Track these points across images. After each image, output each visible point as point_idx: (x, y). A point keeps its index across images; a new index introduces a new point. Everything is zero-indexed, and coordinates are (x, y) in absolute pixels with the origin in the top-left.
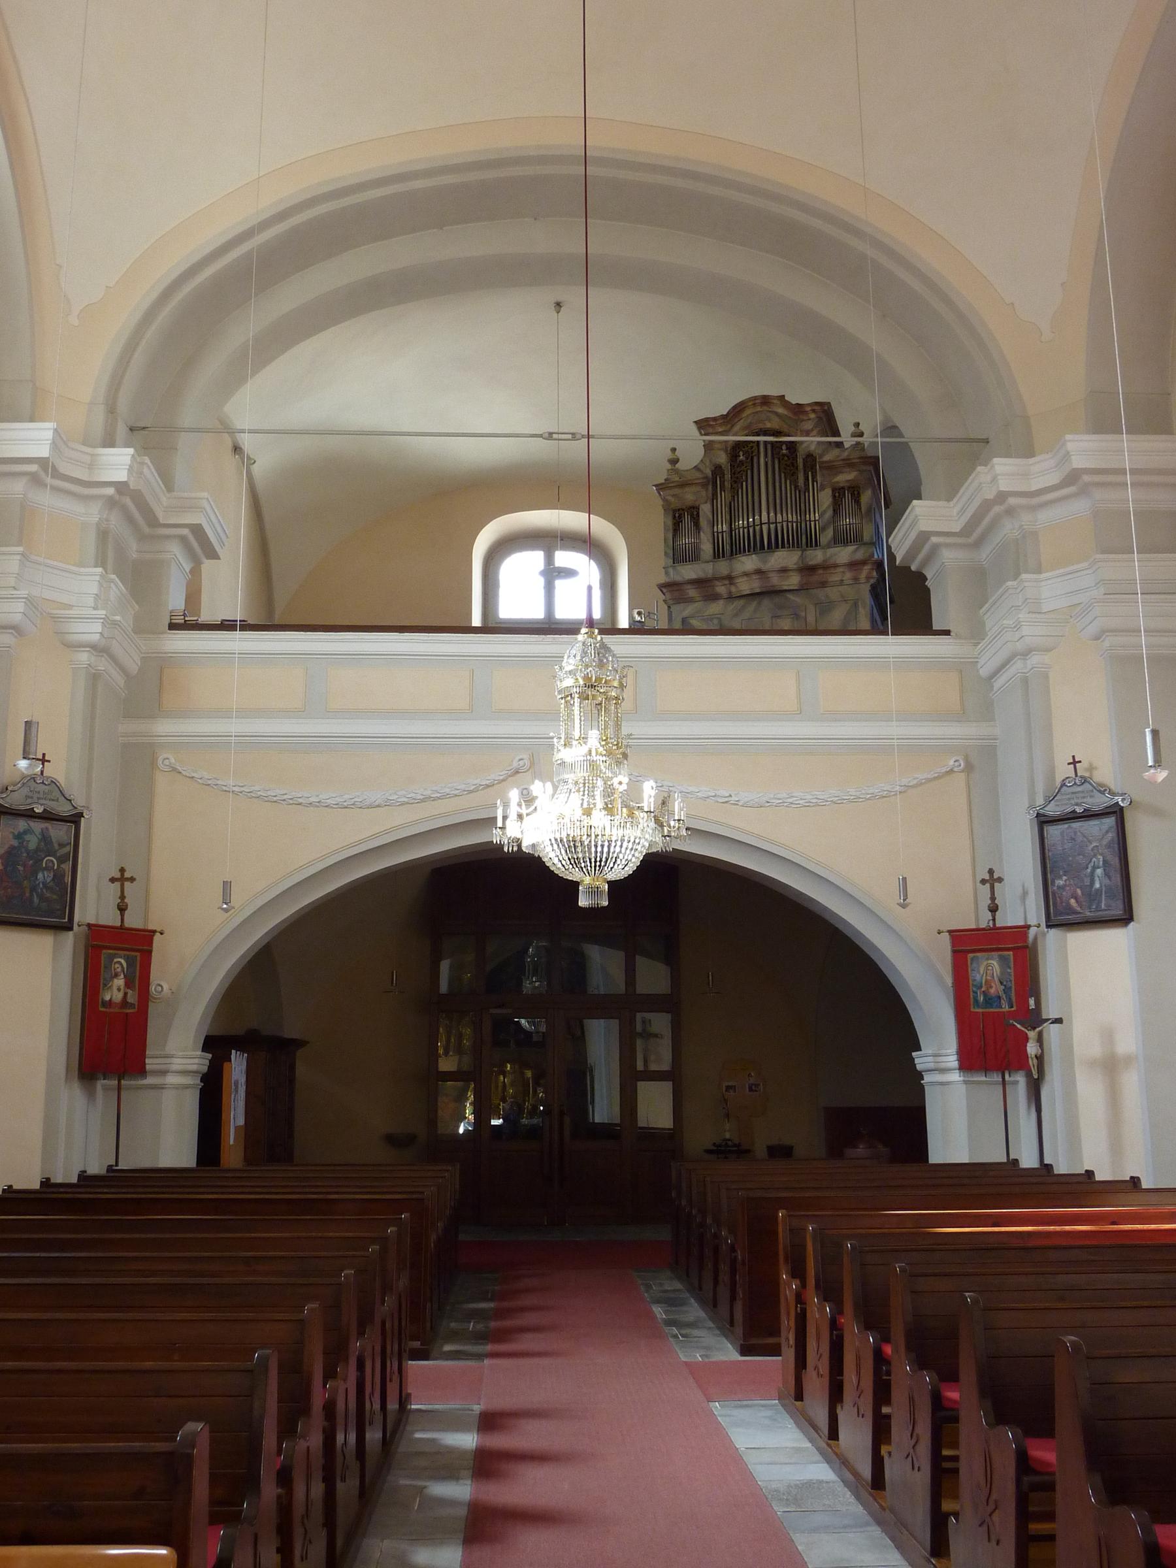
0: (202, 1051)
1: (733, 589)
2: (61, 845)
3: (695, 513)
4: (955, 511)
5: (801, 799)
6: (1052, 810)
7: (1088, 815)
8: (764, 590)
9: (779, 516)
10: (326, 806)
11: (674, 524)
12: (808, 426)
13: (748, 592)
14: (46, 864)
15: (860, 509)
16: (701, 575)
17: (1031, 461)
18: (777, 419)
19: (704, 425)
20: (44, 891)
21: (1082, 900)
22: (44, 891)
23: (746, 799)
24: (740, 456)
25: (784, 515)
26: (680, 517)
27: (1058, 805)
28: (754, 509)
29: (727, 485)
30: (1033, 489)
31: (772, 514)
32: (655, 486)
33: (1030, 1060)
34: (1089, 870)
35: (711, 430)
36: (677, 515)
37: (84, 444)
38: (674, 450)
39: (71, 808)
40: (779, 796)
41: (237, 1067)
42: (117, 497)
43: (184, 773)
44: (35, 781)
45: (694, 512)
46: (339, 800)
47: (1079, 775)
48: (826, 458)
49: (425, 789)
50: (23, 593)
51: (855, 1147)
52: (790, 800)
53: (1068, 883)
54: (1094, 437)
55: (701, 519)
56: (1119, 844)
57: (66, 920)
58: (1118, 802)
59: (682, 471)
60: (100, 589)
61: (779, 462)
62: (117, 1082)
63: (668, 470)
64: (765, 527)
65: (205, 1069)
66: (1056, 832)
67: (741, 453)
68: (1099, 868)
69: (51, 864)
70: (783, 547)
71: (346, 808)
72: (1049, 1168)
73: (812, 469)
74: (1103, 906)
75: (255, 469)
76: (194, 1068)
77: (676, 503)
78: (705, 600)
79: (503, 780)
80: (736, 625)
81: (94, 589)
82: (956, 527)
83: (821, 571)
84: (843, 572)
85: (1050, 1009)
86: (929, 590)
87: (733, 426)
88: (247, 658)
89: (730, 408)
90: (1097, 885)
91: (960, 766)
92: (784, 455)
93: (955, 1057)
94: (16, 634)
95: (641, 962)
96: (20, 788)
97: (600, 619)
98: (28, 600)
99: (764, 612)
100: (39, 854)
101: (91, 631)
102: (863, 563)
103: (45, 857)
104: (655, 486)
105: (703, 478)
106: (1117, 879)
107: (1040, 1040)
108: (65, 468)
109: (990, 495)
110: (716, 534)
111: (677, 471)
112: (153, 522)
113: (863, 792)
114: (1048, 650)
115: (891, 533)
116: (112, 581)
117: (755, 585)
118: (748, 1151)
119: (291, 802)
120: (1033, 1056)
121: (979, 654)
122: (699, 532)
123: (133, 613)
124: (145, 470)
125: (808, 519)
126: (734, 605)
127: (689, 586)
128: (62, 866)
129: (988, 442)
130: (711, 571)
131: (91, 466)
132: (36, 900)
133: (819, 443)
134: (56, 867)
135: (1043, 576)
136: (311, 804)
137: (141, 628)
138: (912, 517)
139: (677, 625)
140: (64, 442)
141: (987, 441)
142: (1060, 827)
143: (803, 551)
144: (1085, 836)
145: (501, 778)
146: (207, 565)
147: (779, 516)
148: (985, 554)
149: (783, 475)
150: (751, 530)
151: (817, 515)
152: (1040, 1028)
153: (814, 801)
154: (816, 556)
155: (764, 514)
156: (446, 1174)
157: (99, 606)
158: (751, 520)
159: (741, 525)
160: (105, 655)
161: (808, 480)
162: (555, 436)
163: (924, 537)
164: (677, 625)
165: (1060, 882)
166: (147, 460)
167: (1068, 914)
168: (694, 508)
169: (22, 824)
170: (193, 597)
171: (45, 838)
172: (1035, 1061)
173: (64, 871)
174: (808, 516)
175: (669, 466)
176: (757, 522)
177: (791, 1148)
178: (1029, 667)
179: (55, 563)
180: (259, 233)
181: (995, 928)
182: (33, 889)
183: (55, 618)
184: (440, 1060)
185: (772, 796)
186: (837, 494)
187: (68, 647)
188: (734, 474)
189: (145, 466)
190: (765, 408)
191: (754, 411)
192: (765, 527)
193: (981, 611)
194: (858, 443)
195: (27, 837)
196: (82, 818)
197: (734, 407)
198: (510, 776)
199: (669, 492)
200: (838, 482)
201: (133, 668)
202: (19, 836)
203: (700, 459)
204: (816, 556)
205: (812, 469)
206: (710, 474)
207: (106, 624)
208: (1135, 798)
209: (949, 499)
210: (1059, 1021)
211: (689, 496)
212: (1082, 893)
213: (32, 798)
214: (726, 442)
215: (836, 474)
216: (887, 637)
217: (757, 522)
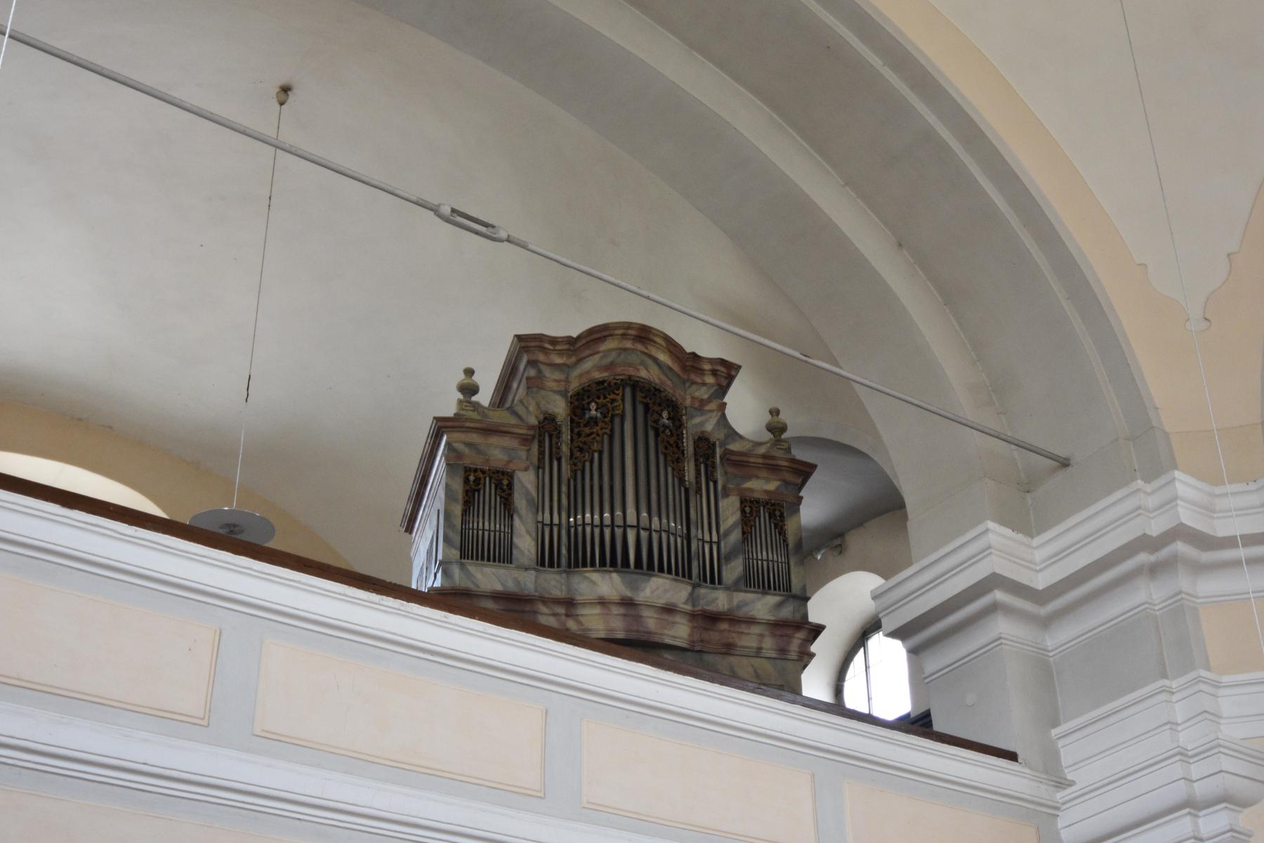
3: (505, 482)
8: (634, 636)
9: (655, 520)
11: (466, 492)
13: (602, 635)
16: (511, 587)
26: (477, 481)
35: (541, 357)
36: (472, 478)
45: (503, 482)
67: (593, 406)
73: (707, 459)
77: (472, 459)
83: (724, 626)
84: (761, 635)
87: (580, 361)
122: (511, 517)
154: (717, 599)
155: (631, 511)
158: (606, 515)
168: (503, 473)
186: (748, 509)
190: (639, 346)
191: (621, 346)
197: (591, 331)
204: (719, 600)
211: (497, 452)
215: (749, 478)
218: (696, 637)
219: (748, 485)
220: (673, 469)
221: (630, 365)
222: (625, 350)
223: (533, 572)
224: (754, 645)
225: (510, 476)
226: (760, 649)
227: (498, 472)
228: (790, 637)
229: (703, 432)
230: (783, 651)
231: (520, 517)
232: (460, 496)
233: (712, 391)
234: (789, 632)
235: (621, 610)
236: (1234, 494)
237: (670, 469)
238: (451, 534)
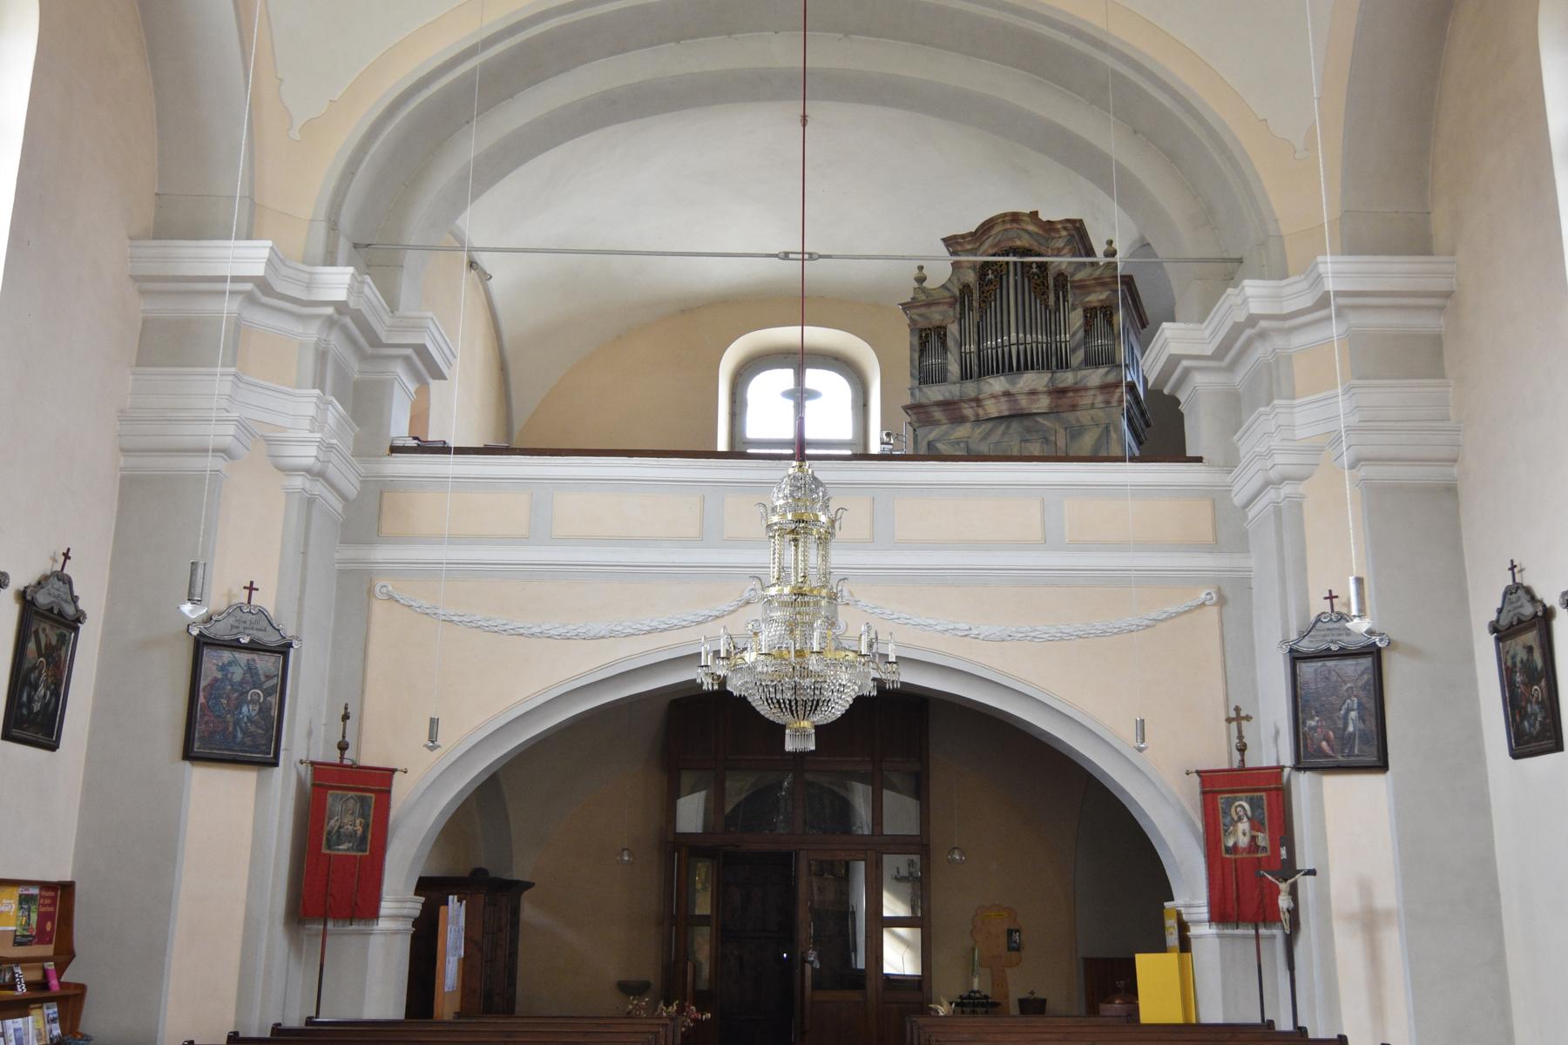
0: (415, 894)
1: (981, 412)
2: (268, 677)
3: (942, 333)
4: (1207, 333)
5: (1045, 633)
6: (1306, 646)
7: (1344, 654)
8: (1013, 412)
9: (1028, 336)
10: (549, 637)
11: (921, 344)
12: (1060, 243)
13: (996, 415)
14: (251, 697)
15: (1113, 330)
16: (948, 396)
17: (1284, 282)
18: (1026, 237)
19: (951, 242)
20: (249, 724)
21: (1334, 743)
22: (249, 724)
23: (987, 634)
24: (988, 275)
25: (1034, 335)
26: (927, 336)
27: (1312, 641)
28: (1003, 330)
29: (975, 304)
30: (1285, 312)
31: (1021, 335)
32: (901, 305)
33: (1282, 914)
34: (1342, 712)
35: (959, 248)
36: (924, 335)
37: (303, 262)
38: (921, 268)
39: (280, 638)
40: (1020, 630)
41: (455, 913)
42: (336, 317)
43: (402, 601)
44: (241, 610)
45: (941, 332)
46: (562, 630)
47: (1335, 610)
48: (1078, 277)
49: (652, 620)
50: (234, 415)
51: (1112, 1002)
52: (1032, 634)
53: (1320, 724)
54: (1341, 258)
55: (948, 339)
56: (1375, 685)
57: (272, 755)
58: (1375, 643)
59: (932, 289)
60: (317, 412)
61: (1029, 281)
62: (322, 927)
63: (915, 289)
64: (1014, 349)
65: (417, 913)
66: (1309, 670)
67: (990, 272)
68: (1353, 710)
69: (256, 697)
70: (1032, 368)
71: (569, 639)
72: (1302, 1031)
73: (1063, 288)
74: (1356, 752)
75: (493, 284)
76: (405, 912)
77: (923, 324)
78: (952, 423)
79: (733, 611)
80: (984, 448)
81: (310, 410)
82: (1209, 351)
83: (1071, 394)
84: (1095, 395)
85: (1304, 860)
86: (1182, 414)
87: (981, 244)
88: (462, 482)
89: (978, 225)
90: (1351, 729)
91: (1212, 599)
92: (1034, 274)
93: (1205, 910)
94: (226, 457)
95: (888, 795)
96: (225, 618)
97: (852, 440)
98: (240, 423)
99: (1012, 437)
100: (244, 685)
101: (307, 455)
102: (1117, 385)
103: (250, 690)
104: (901, 305)
105: (951, 297)
106: (1372, 723)
107: (1293, 892)
108: (280, 286)
109: (1241, 318)
110: (963, 354)
111: (924, 290)
112: (375, 341)
113: (1111, 626)
114: (1301, 479)
115: (1145, 352)
116: (330, 403)
117: (1003, 408)
118: (995, 1005)
119: (512, 632)
120: (1285, 910)
121: (1232, 482)
122: (946, 353)
123: (353, 434)
124: (366, 289)
125: (1058, 340)
126: (981, 429)
127: (935, 408)
128: (268, 699)
129: (1242, 262)
130: (958, 394)
131: (309, 286)
132: (240, 735)
133: (1070, 263)
134: (261, 700)
135: (1296, 402)
136: (532, 634)
137: (362, 451)
138: (1161, 341)
139: (923, 451)
140: (281, 260)
141: (1240, 261)
142: (1313, 664)
143: (1053, 373)
144: (1339, 676)
145: (731, 608)
146: (434, 385)
147: (1028, 336)
148: (1239, 377)
149: (1033, 294)
150: (1000, 351)
151: (1068, 336)
152: (1292, 880)
153: (1060, 635)
154: (1067, 377)
155: (1013, 334)
156: (661, 1029)
157: (316, 429)
158: (999, 340)
159: (989, 346)
160: (320, 479)
161: (1059, 300)
162: (791, 256)
163: (1174, 361)
164: (923, 451)
165: (1313, 723)
166: (368, 279)
167: (1319, 758)
168: (941, 327)
169: (227, 655)
170: (419, 417)
171: (251, 670)
172: (1287, 915)
173: (271, 706)
174: (1058, 337)
175: (916, 285)
176: (1006, 343)
177: (1044, 1001)
178: (1282, 495)
179: (266, 383)
180: (483, 50)
181: (1242, 768)
182: (237, 723)
183: (269, 441)
184: (697, 895)
185: (1014, 629)
186: (1089, 315)
187: (283, 471)
188: (983, 292)
189: (366, 286)
190: (1015, 225)
191: (1004, 228)
192: (1014, 349)
193: (1235, 437)
194: (1109, 263)
195: (231, 669)
196: (291, 649)
197: (983, 225)
198: (741, 607)
199: (914, 311)
200: (1090, 302)
201: (352, 491)
202: (223, 668)
203: (948, 277)
204: (1067, 378)
205: (1063, 288)
206: (958, 294)
207: (322, 447)
208: (1394, 637)
209: (1201, 321)
210: (1312, 872)
211: (936, 316)
212: (1335, 735)
213: (237, 627)
214: (974, 262)
215: (1089, 294)
216: (1123, 464)
217: (1006, 343)
218: (1054, 405)
219: (1089, 298)
220: (1041, 301)
221: (1011, 239)
222: (1006, 230)
223: (959, 385)
224: (1090, 402)
225: (945, 328)
226: (1093, 404)
227: (938, 327)
228: (1113, 392)
229: (1060, 270)
230: (1108, 402)
231: (951, 352)
232: (917, 348)
233: (1066, 240)
234: (1111, 389)
235: (1006, 399)
236: (1296, 282)
237: (1038, 301)
238: (913, 371)
